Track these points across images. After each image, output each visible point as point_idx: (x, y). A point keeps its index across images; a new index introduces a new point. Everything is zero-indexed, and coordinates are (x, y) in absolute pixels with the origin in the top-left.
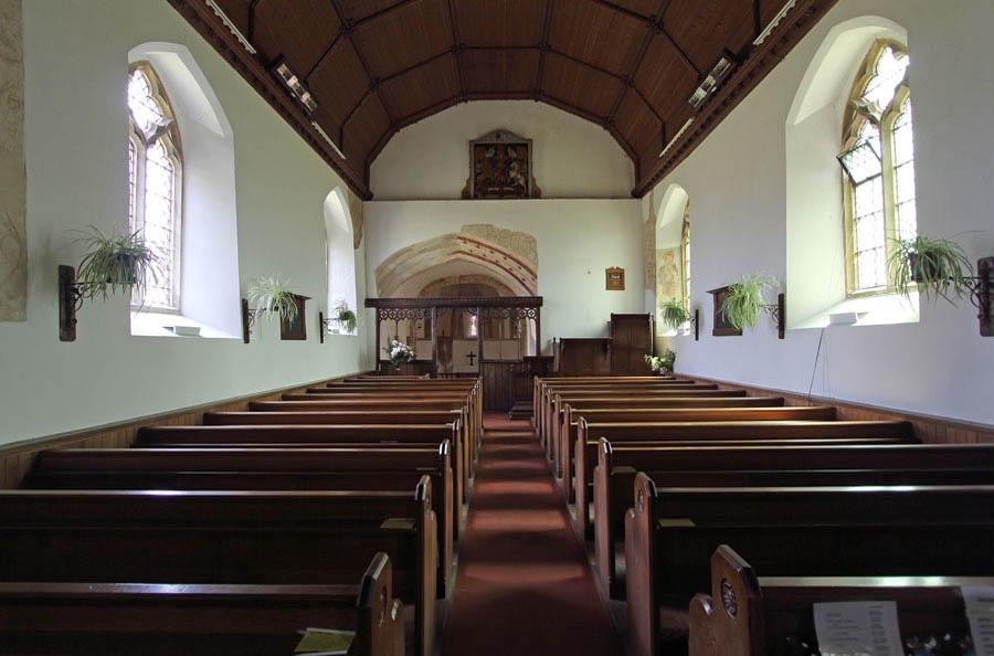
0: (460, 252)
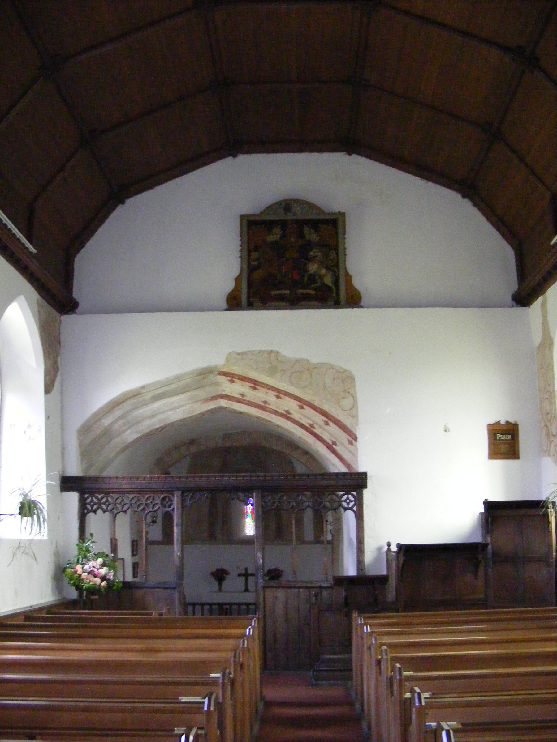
0: (223, 397)
